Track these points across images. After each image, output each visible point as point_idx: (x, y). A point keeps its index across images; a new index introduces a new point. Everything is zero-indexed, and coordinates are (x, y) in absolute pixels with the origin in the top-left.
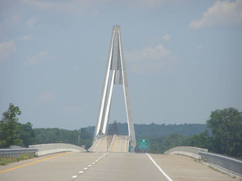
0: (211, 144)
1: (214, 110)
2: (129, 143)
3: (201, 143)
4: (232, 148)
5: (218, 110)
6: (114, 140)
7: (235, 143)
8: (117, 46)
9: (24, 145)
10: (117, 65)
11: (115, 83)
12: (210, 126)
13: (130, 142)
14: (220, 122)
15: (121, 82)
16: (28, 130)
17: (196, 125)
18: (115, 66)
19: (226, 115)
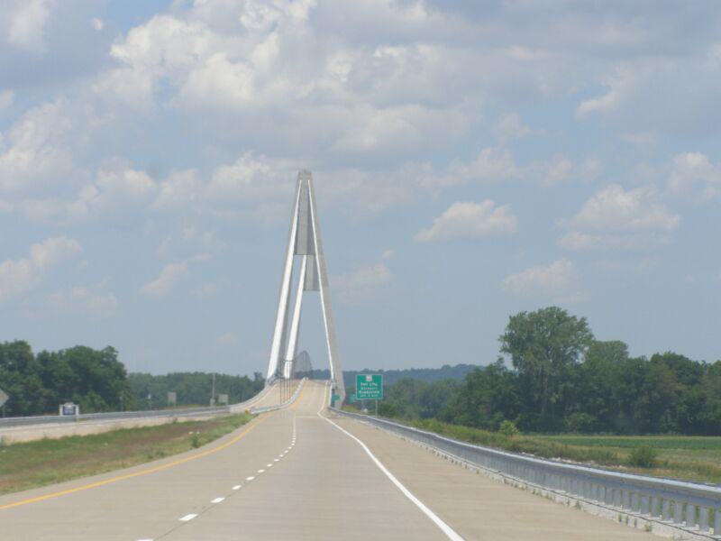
0: (511, 387)
1: (515, 314)
2: (331, 392)
3: (488, 387)
4: (557, 396)
5: (524, 314)
6: (303, 386)
7: (563, 385)
8: (306, 210)
9: (520, 445)
10: (306, 245)
11: (298, 251)
12: (508, 347)
13: (333, 390)
14: (530, 339)
15: (316, 288)
16: (107, 364)
17: (427, 370)
18: (303, 245)
19: (542, 324)
